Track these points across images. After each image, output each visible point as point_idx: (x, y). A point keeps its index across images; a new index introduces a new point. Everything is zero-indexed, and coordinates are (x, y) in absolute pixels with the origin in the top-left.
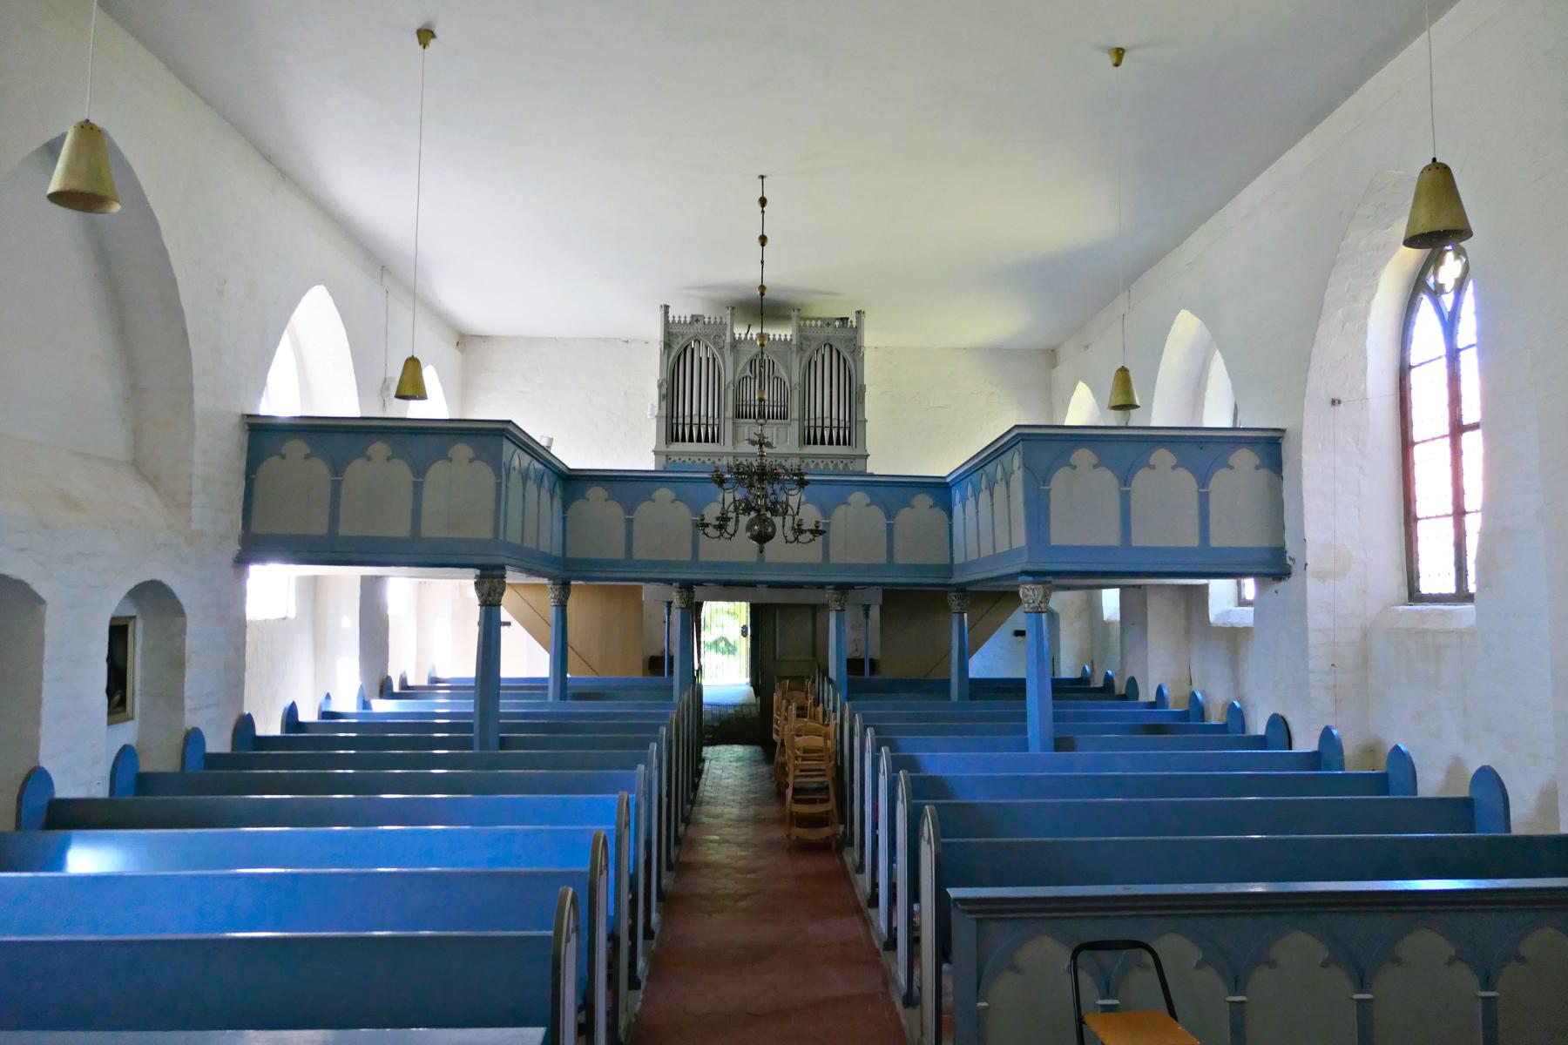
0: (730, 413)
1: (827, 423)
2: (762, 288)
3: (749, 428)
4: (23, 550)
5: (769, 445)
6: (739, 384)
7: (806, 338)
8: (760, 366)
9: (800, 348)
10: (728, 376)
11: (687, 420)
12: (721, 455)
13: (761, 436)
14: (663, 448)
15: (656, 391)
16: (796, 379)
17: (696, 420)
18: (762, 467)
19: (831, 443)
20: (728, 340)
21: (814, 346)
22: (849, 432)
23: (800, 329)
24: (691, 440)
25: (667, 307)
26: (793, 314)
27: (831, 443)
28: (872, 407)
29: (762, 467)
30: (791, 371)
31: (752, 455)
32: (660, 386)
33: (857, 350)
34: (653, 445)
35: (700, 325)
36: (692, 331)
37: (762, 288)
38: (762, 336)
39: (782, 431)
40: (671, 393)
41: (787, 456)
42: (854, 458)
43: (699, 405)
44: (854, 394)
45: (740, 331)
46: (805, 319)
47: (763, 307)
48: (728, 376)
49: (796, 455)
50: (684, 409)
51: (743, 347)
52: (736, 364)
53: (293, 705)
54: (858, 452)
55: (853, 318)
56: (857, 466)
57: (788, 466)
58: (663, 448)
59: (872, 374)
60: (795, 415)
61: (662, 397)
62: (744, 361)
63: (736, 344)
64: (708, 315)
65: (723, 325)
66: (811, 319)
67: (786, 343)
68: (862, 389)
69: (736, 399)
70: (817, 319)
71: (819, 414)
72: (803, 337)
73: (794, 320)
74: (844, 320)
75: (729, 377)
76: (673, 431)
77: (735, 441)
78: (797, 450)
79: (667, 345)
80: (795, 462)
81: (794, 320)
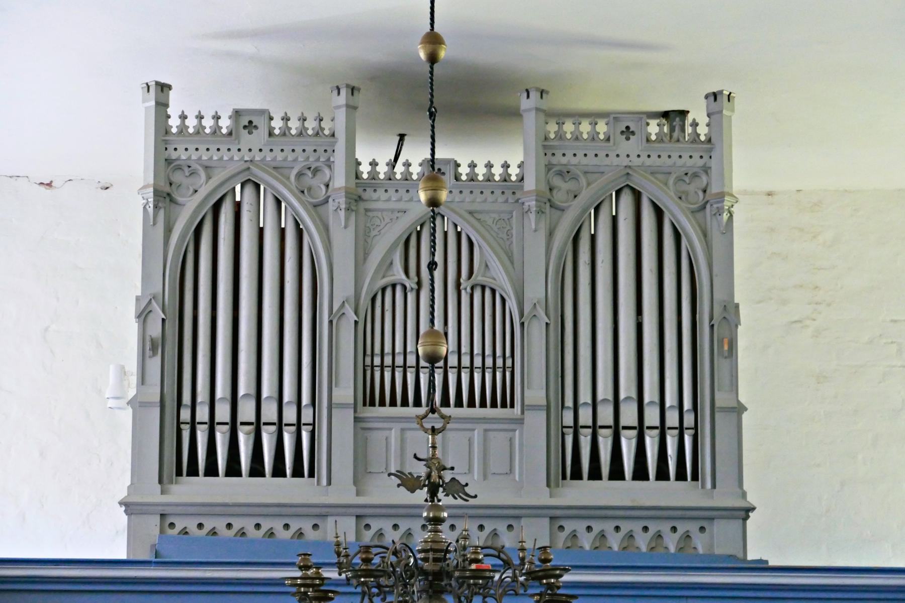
0: (346, 391)
1: (629, 416)
2: (433, 39)
3: (400, 437)
4: (52, 351)
5: (456, 488)
6: (373, 305)
7: (565, 173)
8: (435, 245)
9: (548, 203)
10: (341, 285)
11: (223, 412)
12: (319, 514)
13: (435, 464)
14: (153, 494)
15: (133, 328)
16: (535, 291)
17: (247, 411)
18: (438, 551)
19: (640, 473)
20: (340, 181)
21: (586, 195)
22: (689, 444)
23: (547, 146)
24: (233, 470)
25: (163, 88)
26: (526, 104)
27: (640, 473)
28: (759, 368)
29: (438, 551)
30: (526, 271)
31: (410, 512)
32: (143, 316)
33: (711, 204)
34: (121, 485)
35: (259, 137)
36: (231, 159)
37: (433, 39)
38: (434, 170)
39: (498, 440)
40: (176, 332)
41: (513, 515)
42: (706, 517)
43: (256, 371)
44: (704, 332)
45: (373, 153)
46: (561, 116)
47: (438, 89)
48: (341, 285)
49: (535, 511)
50: (213, 380)
51: (380, 200)
52: (362, 254)
53: (688, 112)
54: (723, 499)
55: (698, 114)
56: (719, 539)
57: (507, 541)
58: (153, 494)
59: (756, 270)
60: (536, 394)
61: (150, 347)
62: (389, 236)
63: (361, 189)
64: (281, 107)
65: (324, 137)
66: (578, 116)
67: (509, 186)
68: (730, 315)
69: (364, 349)
70: (594, 116)
71: (604, 390)
72: (554, 166)
73: (530, 120)
74: (674, 117)
75: (344, 287)
76: (181, 452)
77: (361, 471)
78: (539, 495)
79: (164, 198)
80: (534, 535)
81: (530, 120)
